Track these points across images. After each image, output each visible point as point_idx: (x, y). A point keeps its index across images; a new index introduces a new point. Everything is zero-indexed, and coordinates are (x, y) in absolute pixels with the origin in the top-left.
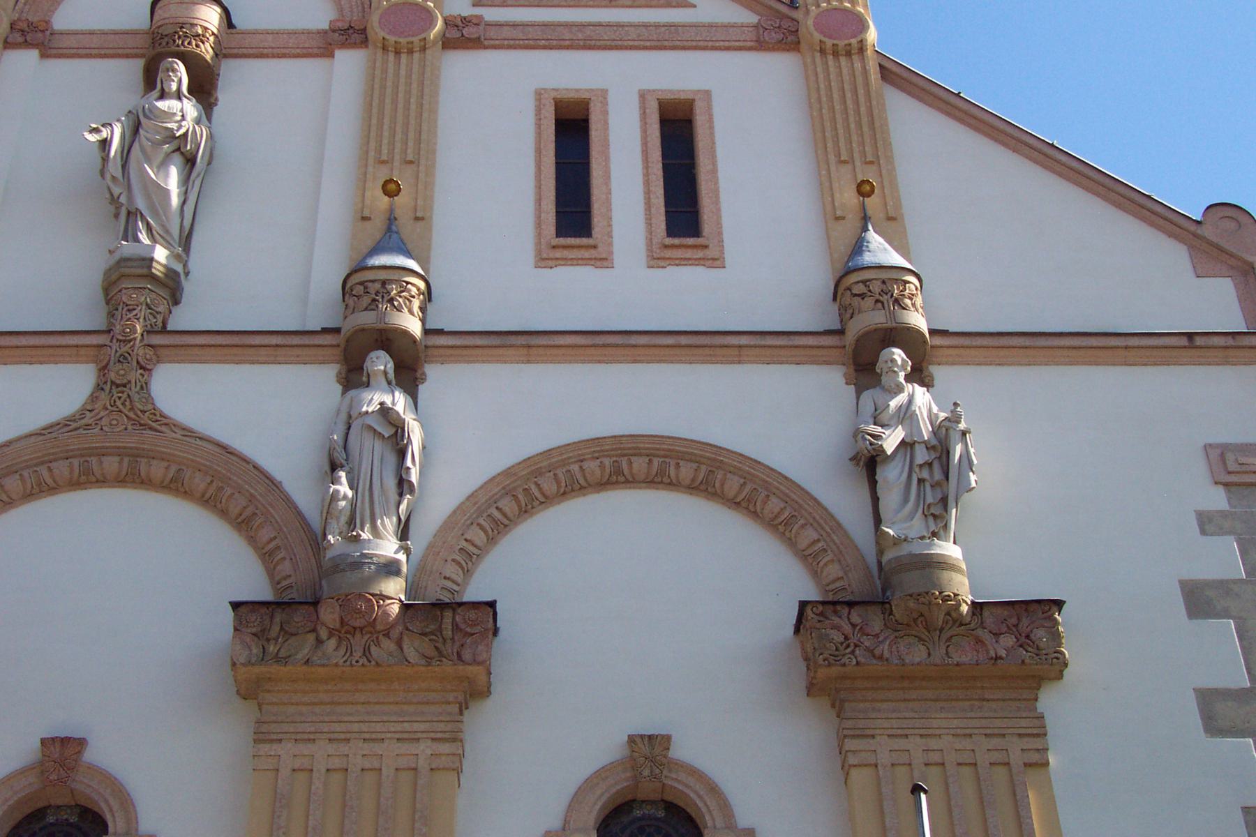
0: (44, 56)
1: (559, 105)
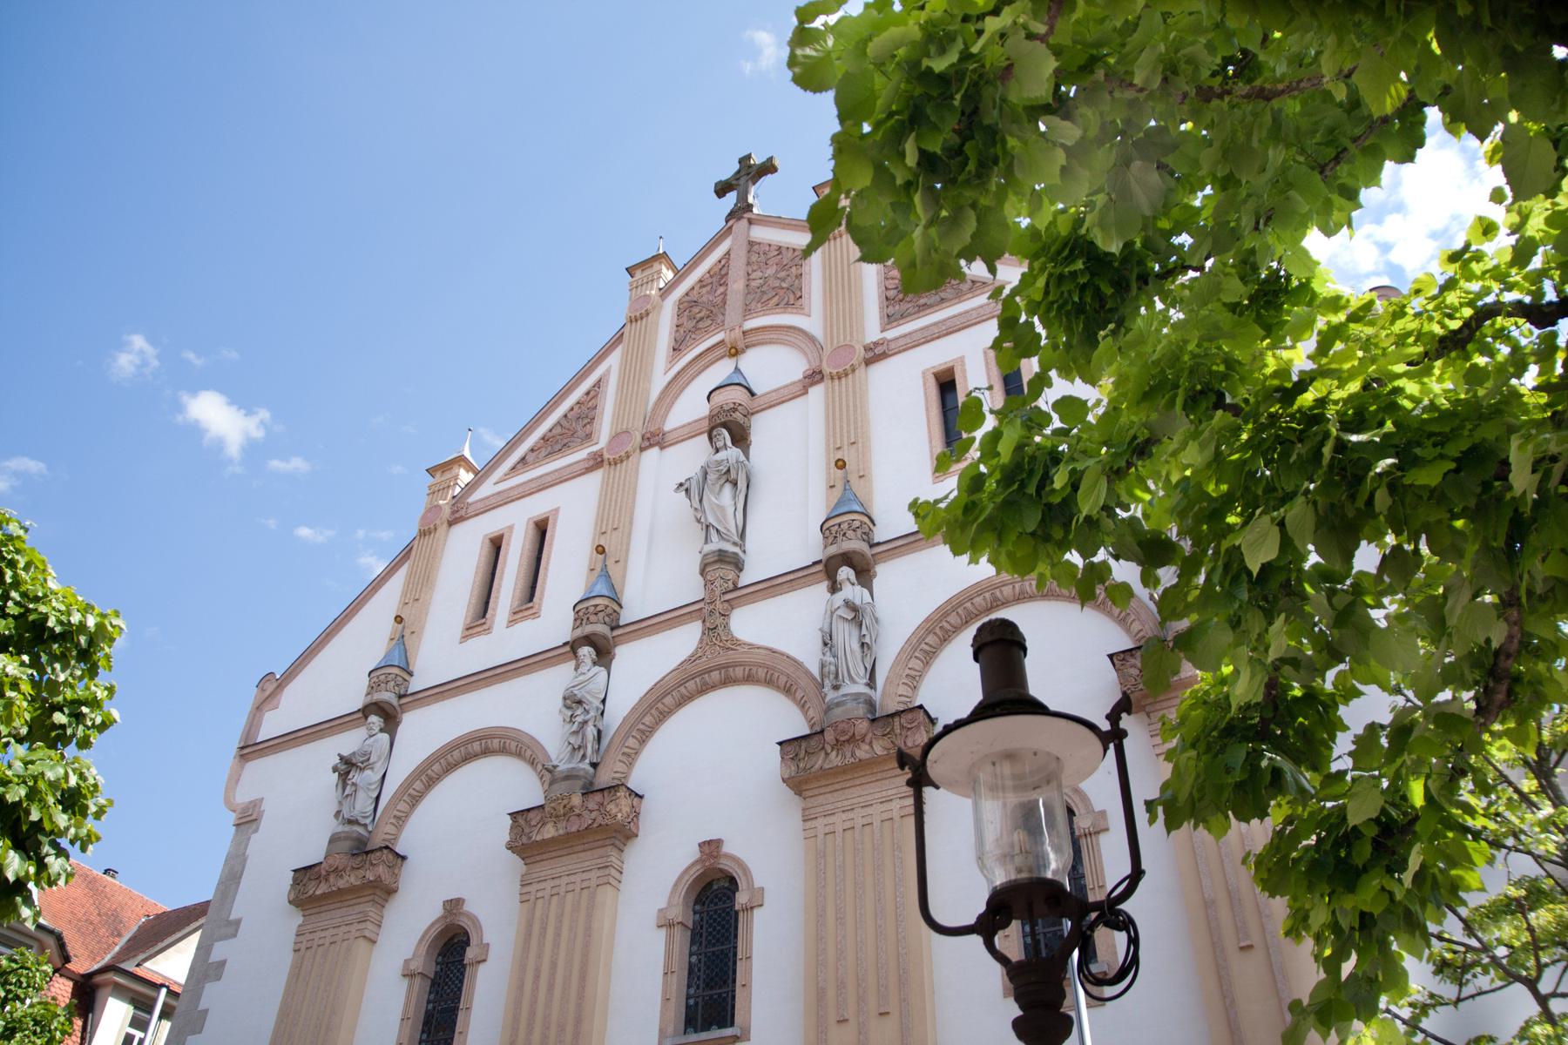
0: (662, 448)
1: (937, 376)
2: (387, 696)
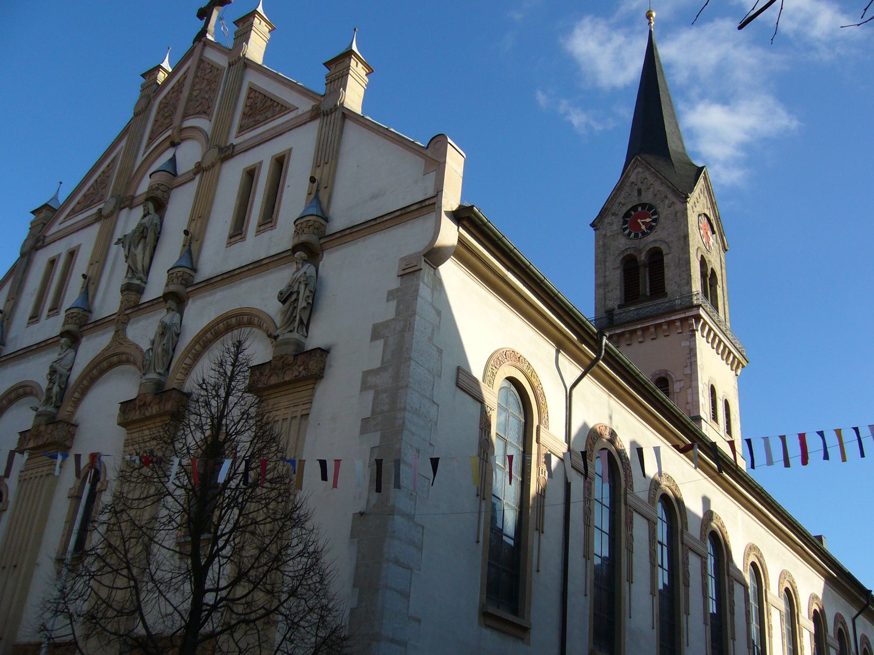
2: (313, 239)
